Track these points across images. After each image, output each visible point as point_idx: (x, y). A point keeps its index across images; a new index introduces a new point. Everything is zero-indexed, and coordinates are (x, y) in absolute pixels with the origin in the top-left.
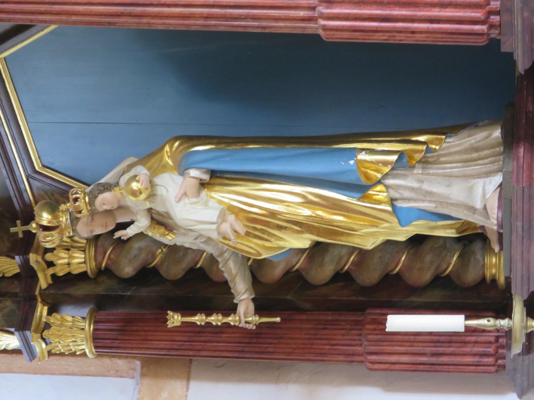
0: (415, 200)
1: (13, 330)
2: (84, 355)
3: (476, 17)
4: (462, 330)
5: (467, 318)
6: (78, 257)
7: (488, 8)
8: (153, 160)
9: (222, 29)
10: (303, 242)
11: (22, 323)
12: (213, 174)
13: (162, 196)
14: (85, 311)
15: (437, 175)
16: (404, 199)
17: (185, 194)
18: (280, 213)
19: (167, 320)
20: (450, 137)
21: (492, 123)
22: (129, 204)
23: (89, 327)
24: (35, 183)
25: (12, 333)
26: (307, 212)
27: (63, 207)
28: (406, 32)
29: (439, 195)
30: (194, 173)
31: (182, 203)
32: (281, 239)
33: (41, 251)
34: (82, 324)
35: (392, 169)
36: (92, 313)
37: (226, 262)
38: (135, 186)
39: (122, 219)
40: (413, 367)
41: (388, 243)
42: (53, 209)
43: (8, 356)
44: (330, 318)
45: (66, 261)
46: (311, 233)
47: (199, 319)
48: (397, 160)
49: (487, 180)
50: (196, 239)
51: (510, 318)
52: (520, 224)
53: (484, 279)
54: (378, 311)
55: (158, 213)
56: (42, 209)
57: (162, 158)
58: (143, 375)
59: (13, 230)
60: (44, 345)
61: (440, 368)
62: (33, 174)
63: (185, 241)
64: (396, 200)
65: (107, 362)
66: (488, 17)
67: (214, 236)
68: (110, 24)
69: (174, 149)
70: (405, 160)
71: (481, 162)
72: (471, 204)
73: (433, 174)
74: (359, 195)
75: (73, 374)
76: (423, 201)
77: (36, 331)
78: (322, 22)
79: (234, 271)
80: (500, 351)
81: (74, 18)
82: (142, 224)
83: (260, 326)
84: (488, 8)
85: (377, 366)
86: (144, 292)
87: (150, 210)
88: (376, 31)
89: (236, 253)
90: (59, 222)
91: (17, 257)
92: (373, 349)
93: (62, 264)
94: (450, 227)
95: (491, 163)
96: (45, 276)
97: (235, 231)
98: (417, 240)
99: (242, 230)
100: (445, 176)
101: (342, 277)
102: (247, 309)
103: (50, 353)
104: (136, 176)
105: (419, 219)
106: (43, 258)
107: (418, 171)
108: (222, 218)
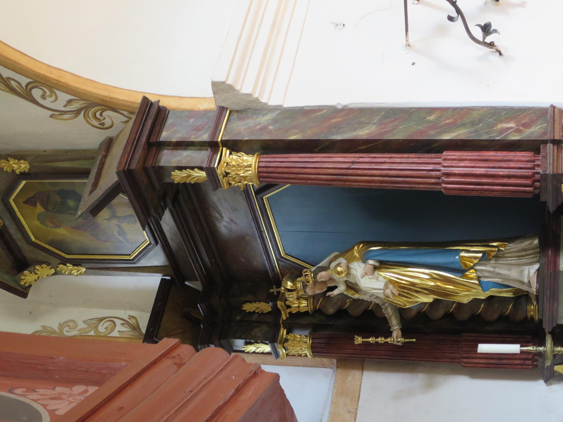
0: (491, 277)
1: (268, 342)
2: (306, 356)
3: (526, 183)
4: (519, 352)
5: (521, 346)
6: (304, 303)
7: (533, 179)
8: (348, 254)
9: (389, 188)
10: (428, 299)
11: (272, 339)
12: (381, 262)
13: (353, 274)
14: (307, 333)
15: (503, 264)
16: (485, 277)
17: (366, 274)
18: (417, 284)
19: (354, 340)
20: (511, 243)
21: (532, 237)
22: (335, 278)
23: (309, 341)
24: (281, 263)
25: (267, 344)
26: (432, 284)
27: (299, 279)
28: (489, 191)
29: (504, 275)
30: (371, 262)
31: (364, 278)
32: (417, 297)
33: (284, 300)
34: (305, 340)
35: (479, 261)
36: (310, 334)
37: (386, 308)
38: (339, 269)
39: (331, 285)
40: (488, 366)
41: (475, 300)
42: (293, 281)
43: (264, 355)
44: (441, 338)
45: (297, 305)
46: (434, 294)
47: (371, 340)
48: (482, 256)
49: (530, 267)
50: (371, 296)
51: (545, 346)
52: (548, 292)
53: (527, 317)
54: (467, 334)
55: (351, 283)
56: (287, 280)
57: (353, 253)
58: (338, 367)
59: (271, 291)
60: (284, 351)
61: (502, 366)
62: (280, 258)
63: (365, 298)
64: (481, 277)
65: (318, 359)
66: (533, 183)
67: (382, 296)
68: (329, 185)
69: (360, 248)
70: (486, 256)
71: (527, 257)
72: (522, 280)
73: (501, 264)
74: (460, 275)
75: (299, 366)
76: (496, 278)
77: (280, 343)
78: (444, 185)
79: (391, 314)
80: (535, 357)
81: (309, 182)
82: (341, 289)
83: (404, 343)
84: (533, 179)
85: (467, 365)
87: (346, 282)
88: (473, 190)
89: (392, 305)
90: (297, 287)
91: (270, 303)
92: (465, 355)
93: (295, 307)
94: (510, 291)
95: (533, 258)
96: (286, 314)
97: (393, 294)
98: (491, 298)
99: (396, 292)
100: (507, 264)
101: (448, 316)
102: (398, 334)
103: (287, 355)
104: (340, 264)
105: (493, 287)
106: (285, 304)
107: (493, 262)
108: (386, 287)
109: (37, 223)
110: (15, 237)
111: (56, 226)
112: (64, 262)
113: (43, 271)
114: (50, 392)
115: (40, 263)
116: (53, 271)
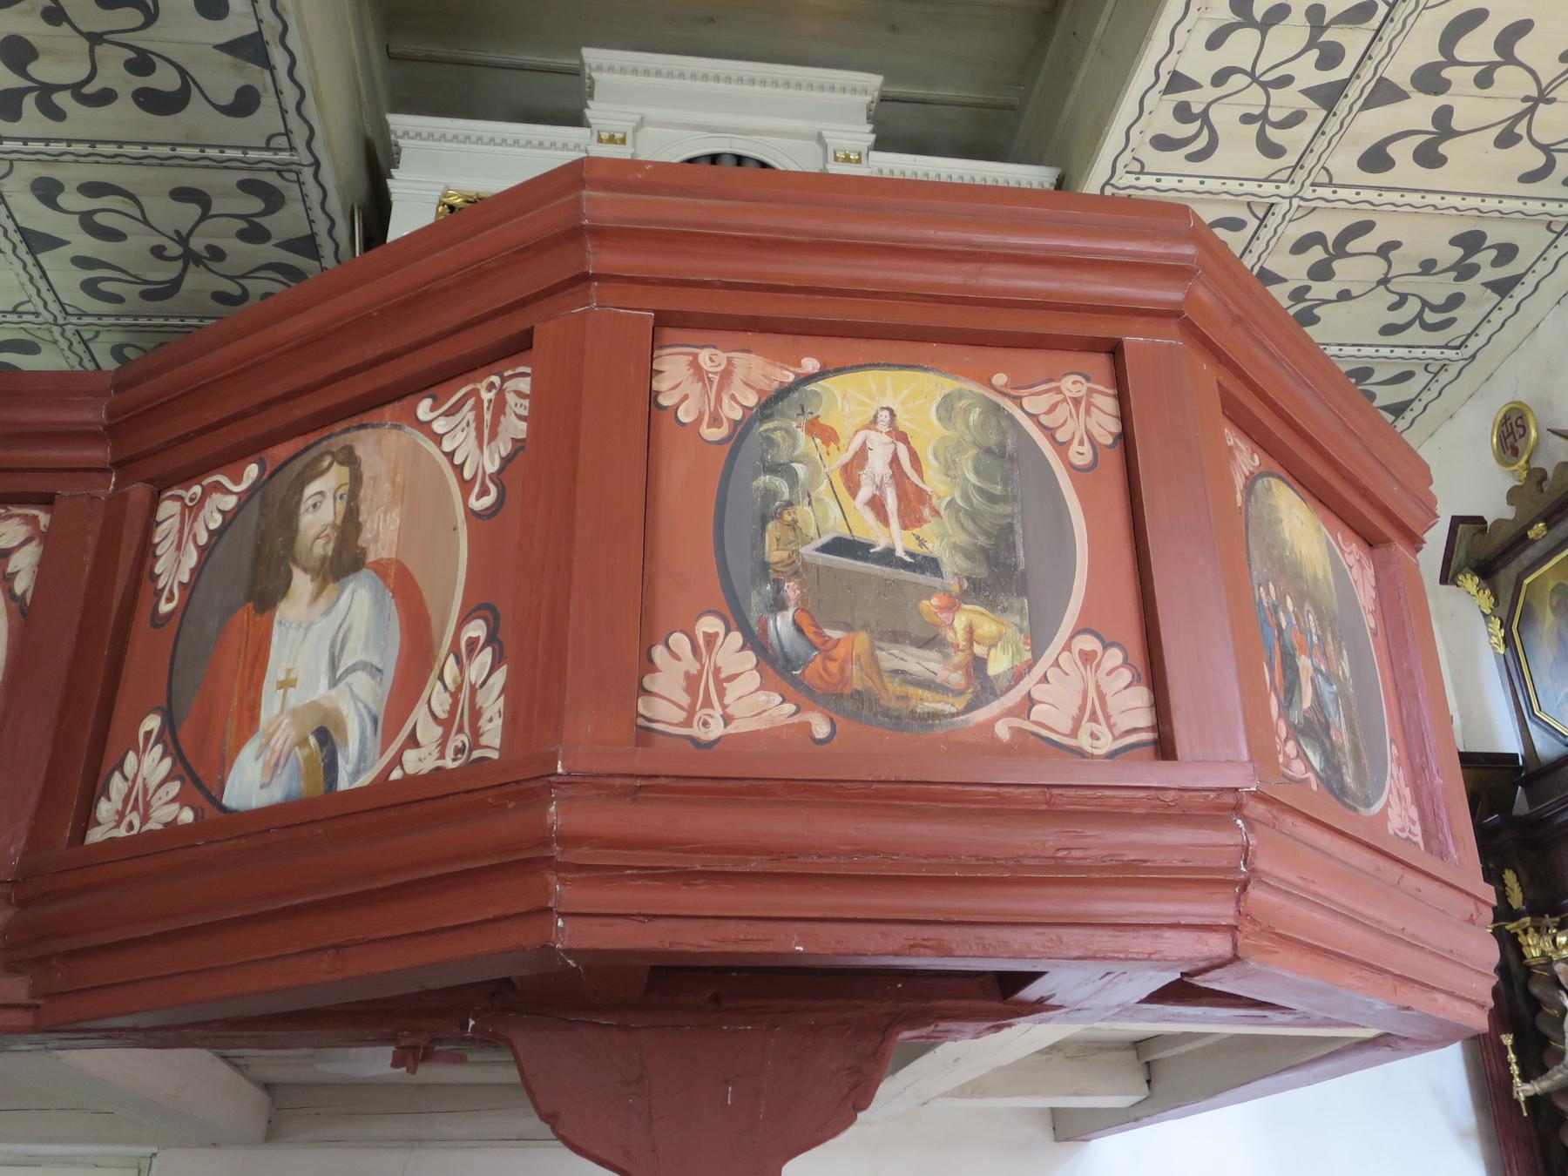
47: (1512, 1057)
83: (1517, 1102)
86: (1522, 1005)
109: (1551, 584)
110: (1522, 556)
111: (1554, 610)
112: (1506, 625)
113: (1485, 601)
114: (1403, 783)
115: (1495, 594)
116: (1488, 611)
